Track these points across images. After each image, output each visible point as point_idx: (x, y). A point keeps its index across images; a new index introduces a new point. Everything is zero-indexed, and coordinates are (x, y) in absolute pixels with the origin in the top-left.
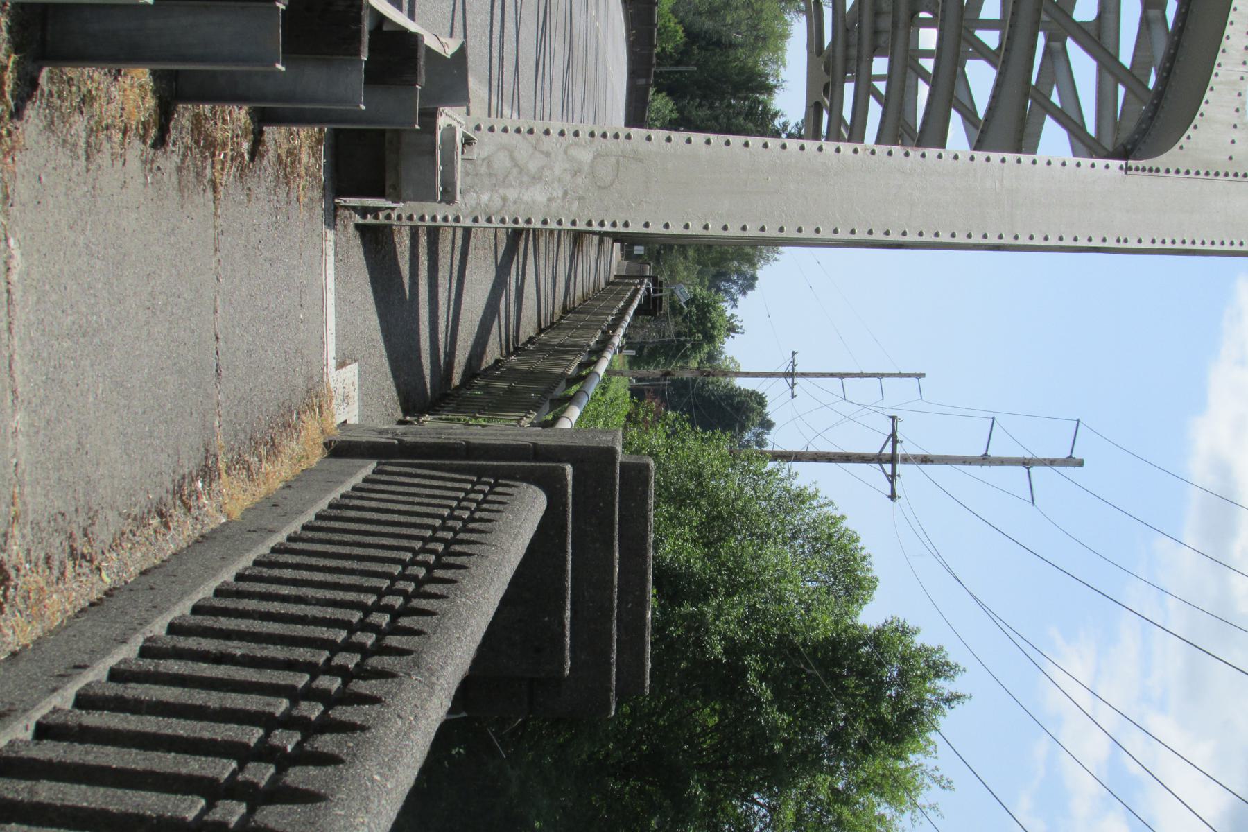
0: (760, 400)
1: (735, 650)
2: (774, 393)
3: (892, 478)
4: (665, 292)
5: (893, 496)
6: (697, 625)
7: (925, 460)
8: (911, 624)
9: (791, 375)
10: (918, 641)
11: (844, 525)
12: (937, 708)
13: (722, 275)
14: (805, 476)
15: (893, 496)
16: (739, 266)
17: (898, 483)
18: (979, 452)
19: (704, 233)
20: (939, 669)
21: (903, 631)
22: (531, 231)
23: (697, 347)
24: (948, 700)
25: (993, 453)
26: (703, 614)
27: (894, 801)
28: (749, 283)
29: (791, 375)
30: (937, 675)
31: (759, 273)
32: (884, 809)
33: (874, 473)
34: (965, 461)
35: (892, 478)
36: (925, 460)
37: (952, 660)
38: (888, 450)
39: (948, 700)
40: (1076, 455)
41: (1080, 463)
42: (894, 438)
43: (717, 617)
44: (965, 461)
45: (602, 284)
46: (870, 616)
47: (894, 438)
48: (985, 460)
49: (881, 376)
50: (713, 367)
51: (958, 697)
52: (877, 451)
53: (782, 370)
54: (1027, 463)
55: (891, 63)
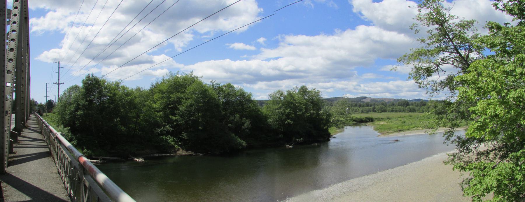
0: (49, 101)
1: (87, 101)
2: (49, 99)
3: (61, 83)
4: (37, 110)
5: (64, 83)
6: (83, 106)
7: (59, 79)
8: (82, 80)
9: (47, 97)
10: (85, 79)
11: (68, 88)
12: (94, 77)
13: (35, 104)
14: (61, 93)
15: (64, 83)
16: (137, 120)
17: (62, 83)
18: (58, 74)
19: (10, 110)
20: (88, 76)
21: (83, 81)
22: (9, 160)
23: (43, 106)
24: (93, 75)
25: (58, 72)
26: (82, 105)
27: (105, 82)
28: (36, 102)
29: (47, 97)
30: (90, 77)
31: (36, 101)
32: (106, 84)
33: (60, 86)
34: (59, 75)
35: (61, 83)
36: (59, 79)
37: (87, 75)
38: (58, 84)
39: (93, 75)
40: (58, 62)
41: (59, 62)
42: (56, 83)
43: (82, 103)
44: (59, 75)
45: (36, 119)
46: (81, 85)
47: (56, 83)
48: (59, 73)
49: (47, 88)
50: (45, 105)
51: (92, 74)
52: (58, 85)
53: (57, 86)
54: (59, 68)
55: (6, 85)
